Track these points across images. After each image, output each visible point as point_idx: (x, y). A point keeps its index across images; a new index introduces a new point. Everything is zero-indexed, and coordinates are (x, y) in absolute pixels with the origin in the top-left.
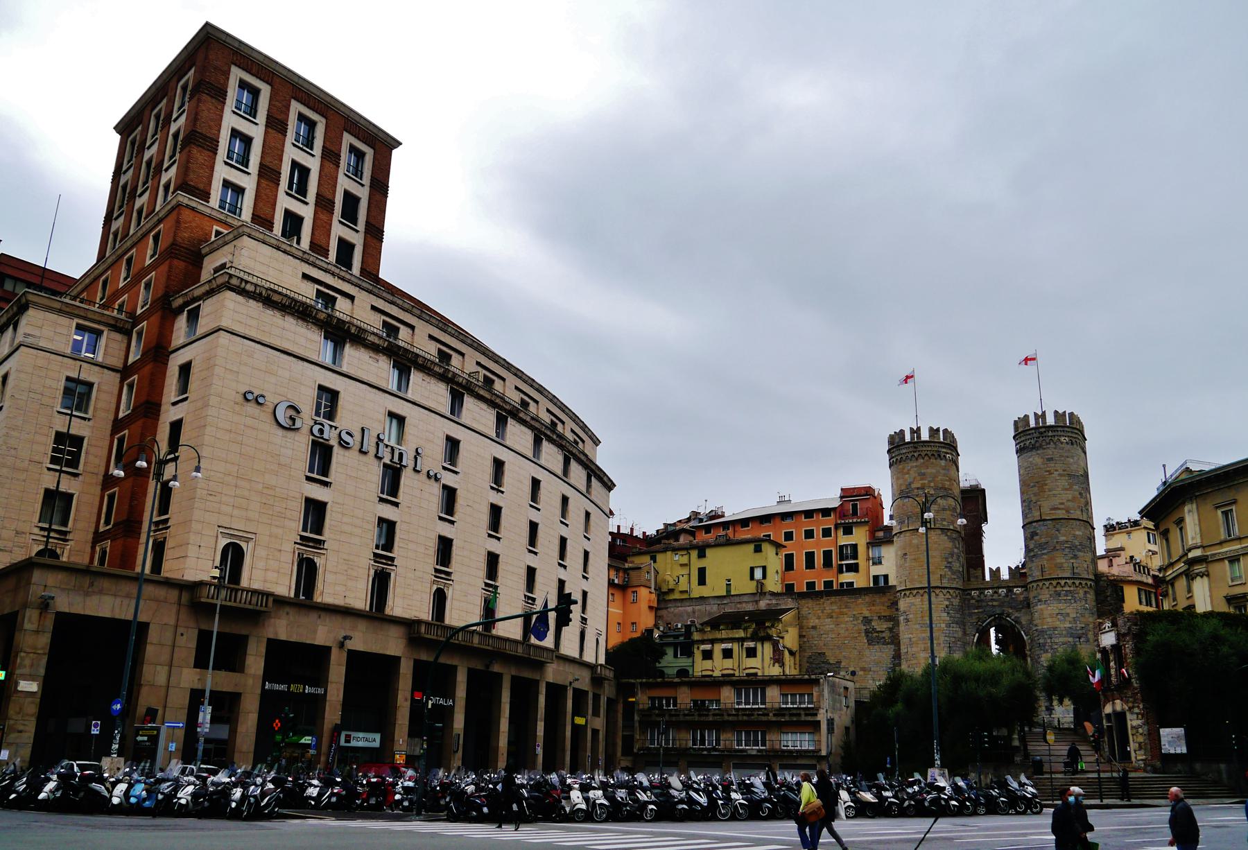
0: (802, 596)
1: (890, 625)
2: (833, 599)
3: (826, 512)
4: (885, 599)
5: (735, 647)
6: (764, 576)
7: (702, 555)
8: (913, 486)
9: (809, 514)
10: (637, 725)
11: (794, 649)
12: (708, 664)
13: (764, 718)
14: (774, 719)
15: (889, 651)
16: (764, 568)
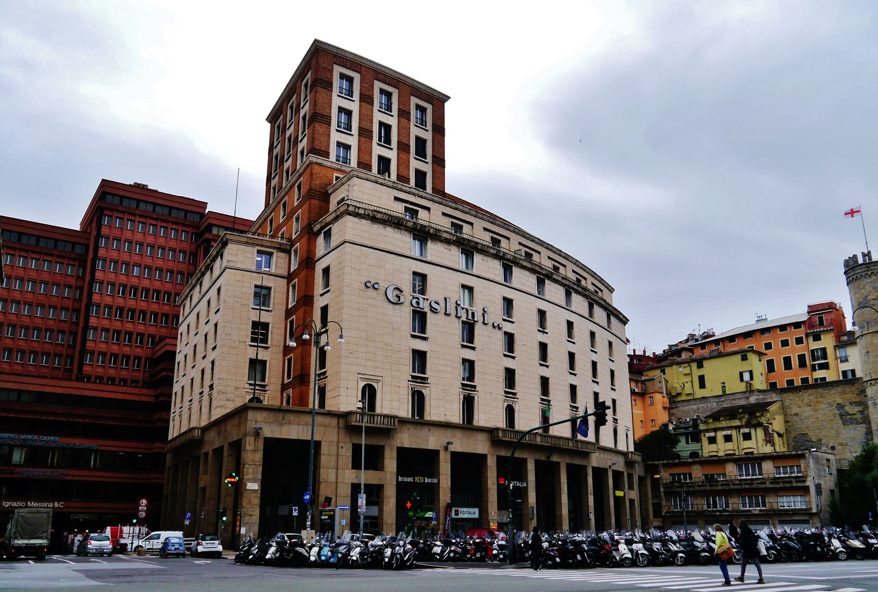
0: (783, 391)
1: (861, 408)
2: (810, 391)
3: (797, 325)
4: (854, 388)
5: (734, 433)
6: (752, 378)
7: (700, 366)
8: (869, 298)
9: (783, 328)
10: (662, 494)
11: (782, 432)
12: (713, 447)
13: (762, 486)
14: (771, 486)
15: (862, 429)
16: (751, 372)
